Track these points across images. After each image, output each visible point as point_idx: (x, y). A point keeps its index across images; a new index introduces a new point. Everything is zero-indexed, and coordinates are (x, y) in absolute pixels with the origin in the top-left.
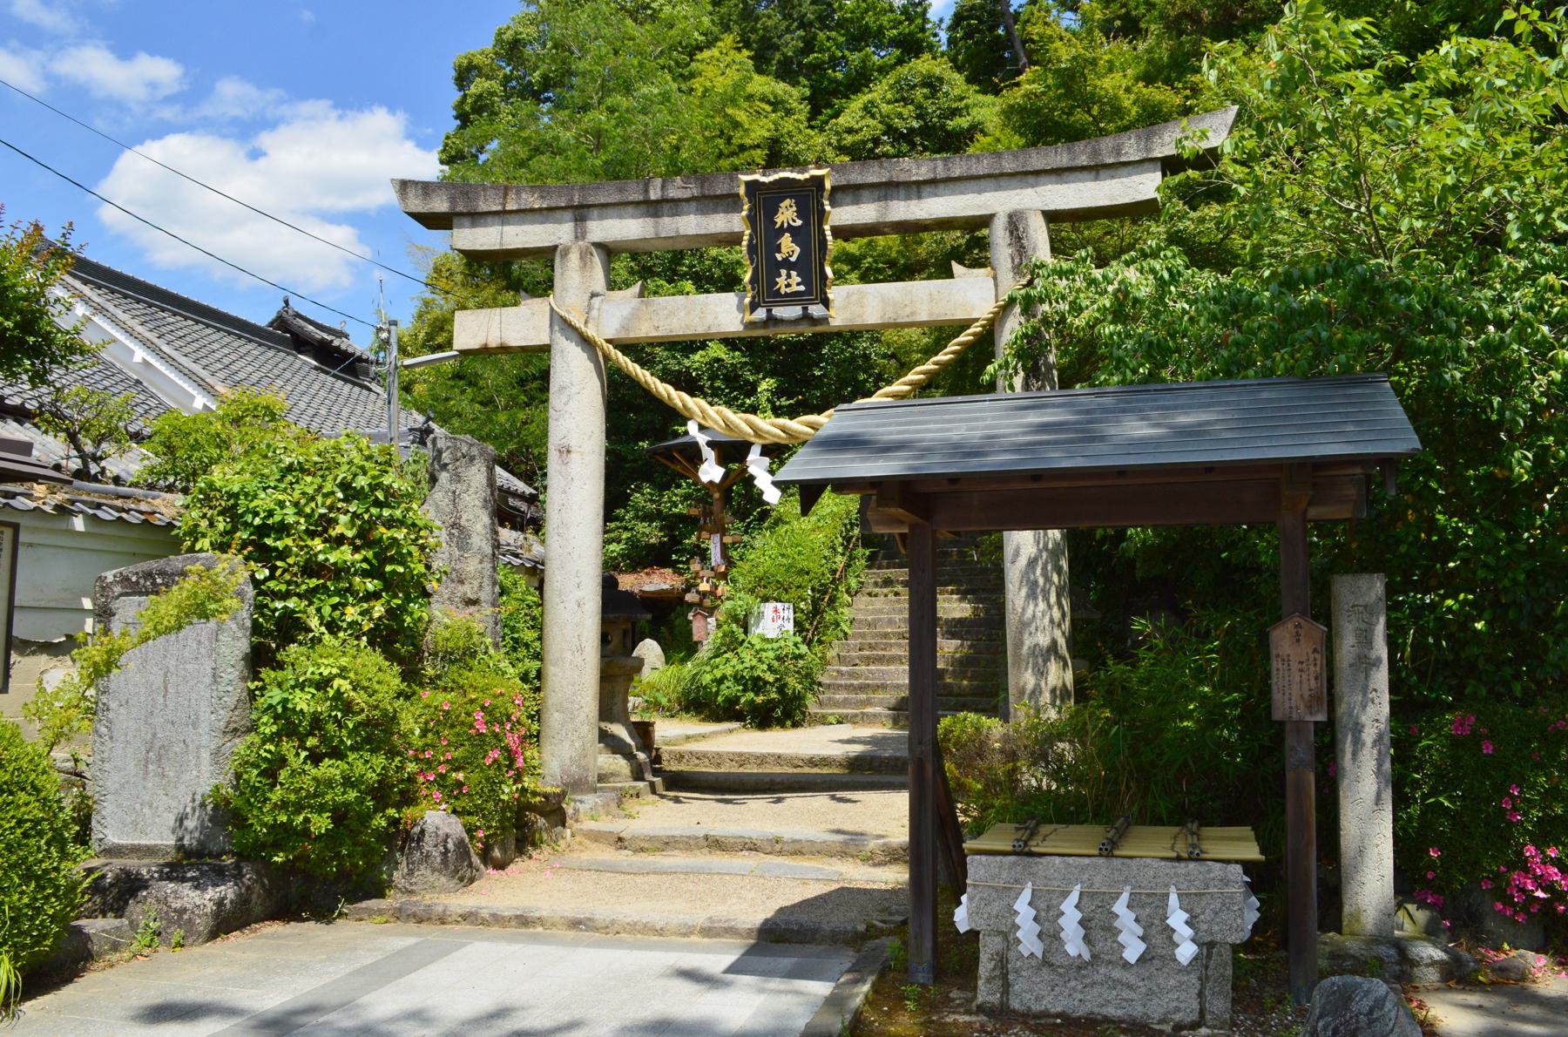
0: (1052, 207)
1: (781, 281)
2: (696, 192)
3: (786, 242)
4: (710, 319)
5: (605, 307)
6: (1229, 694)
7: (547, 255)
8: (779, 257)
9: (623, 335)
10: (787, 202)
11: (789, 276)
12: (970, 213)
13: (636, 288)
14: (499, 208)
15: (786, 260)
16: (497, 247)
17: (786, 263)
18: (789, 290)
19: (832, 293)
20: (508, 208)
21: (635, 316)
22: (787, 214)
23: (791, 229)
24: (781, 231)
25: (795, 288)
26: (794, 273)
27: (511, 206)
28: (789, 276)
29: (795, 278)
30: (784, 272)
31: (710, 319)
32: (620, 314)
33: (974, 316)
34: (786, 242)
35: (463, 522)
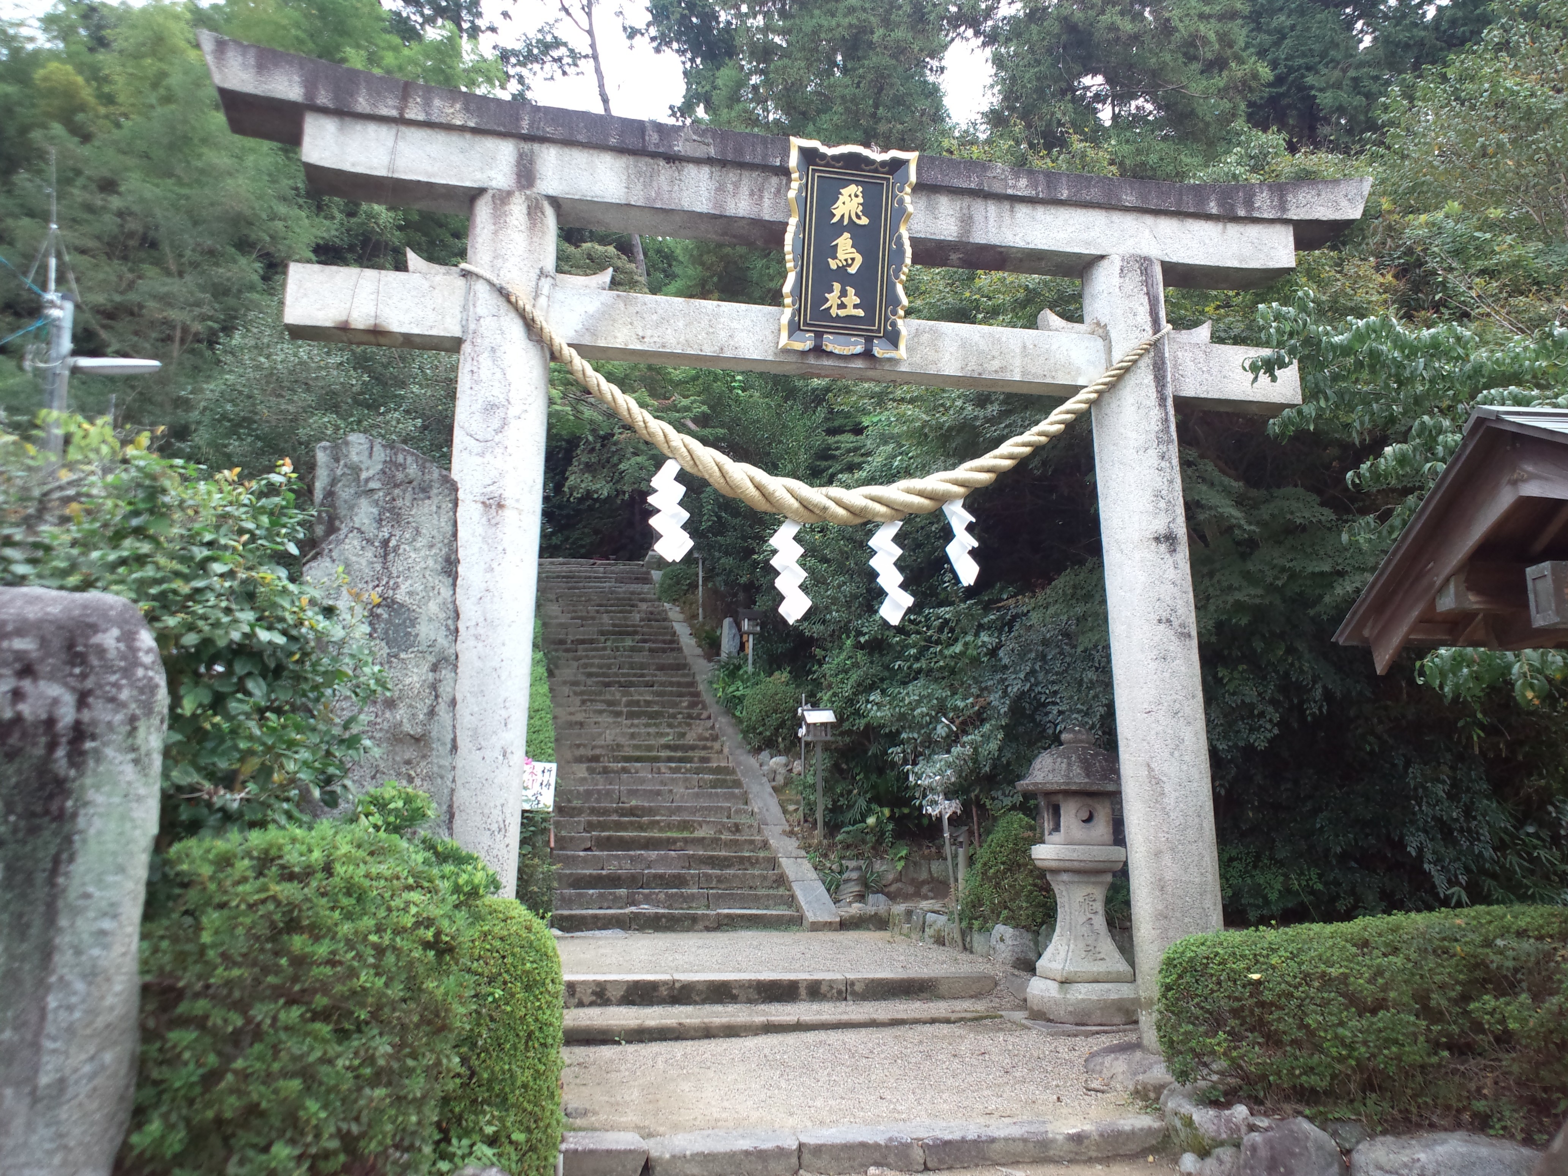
0: (1174, 259)
1: (833, 298)
2: (712, 151)
3: (845, 245)
4: (723, 335)
5: (559, 295)
6: (1433, 337)
7: (1079, 267)
8: (833, 264)
9: (587, 341)
10: (853, 189)
11: (843, 293)
12: (1077, 250)
13: (606, 276)
14: (394, 113)
15: (842, 270)
16: (382, 172)
17: (842, 274)
18: (842, 313)
19: (906, 327)
20: (410, 115)
21: (606, 314)
22: (849, 203)
23: (852, 227)
24: (839, 228)
25: (851, 311)
26: (851, 291)
27: (414, 113)
28: (843, 293)
29: (852, 298)
30: (837, 286)
31: (723, 335)
32: (578, 308)
33: (1080, 382)
34: (845, 245)
35: (401, 596)
